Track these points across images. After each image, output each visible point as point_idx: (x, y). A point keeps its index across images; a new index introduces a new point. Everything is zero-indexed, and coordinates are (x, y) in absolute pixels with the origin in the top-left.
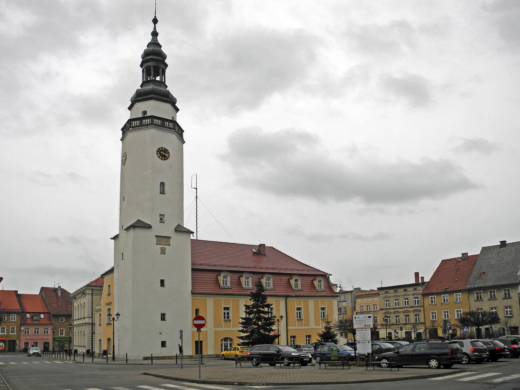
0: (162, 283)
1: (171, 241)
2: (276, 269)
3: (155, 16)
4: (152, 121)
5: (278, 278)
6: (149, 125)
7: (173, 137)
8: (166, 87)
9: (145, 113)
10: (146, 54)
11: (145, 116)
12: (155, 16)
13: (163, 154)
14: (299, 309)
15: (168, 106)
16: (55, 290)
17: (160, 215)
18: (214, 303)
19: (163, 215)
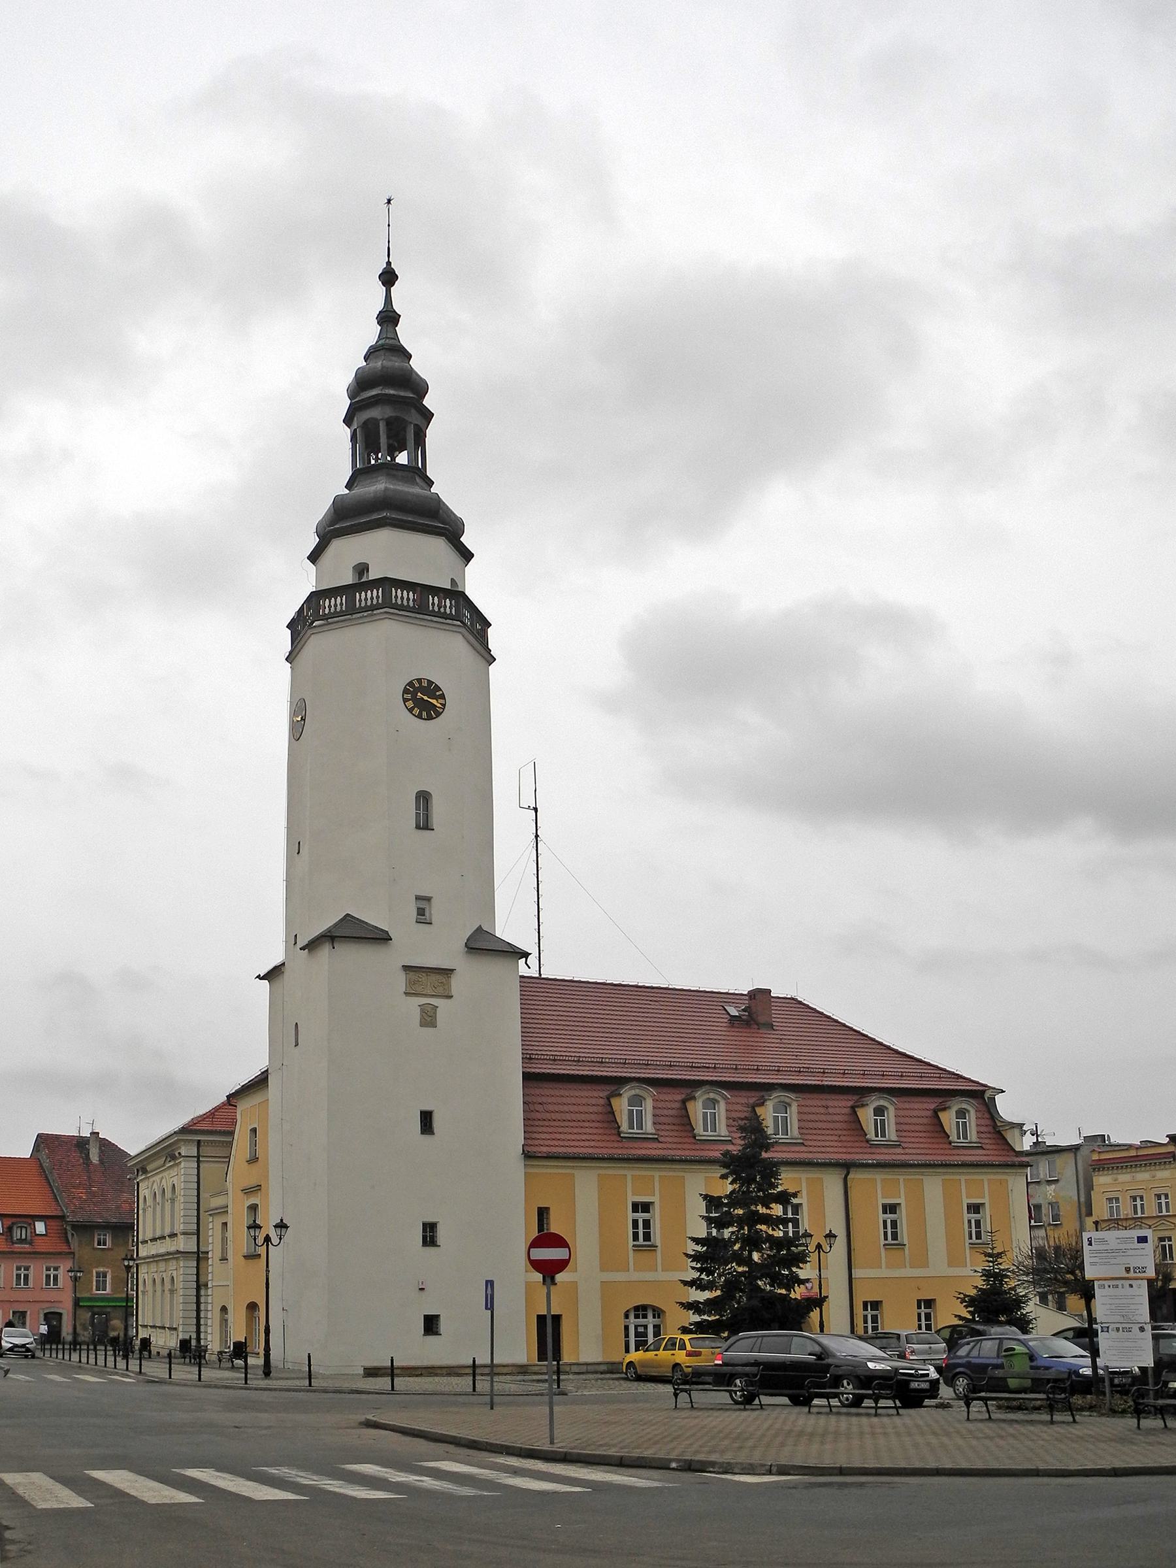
0: (427, 1121)
2: (809, 1071)
3: (389, 263)
8: (430, 483)
9: (362, 569)
10: (362, 384)
11: (362, 581)
12: (389, 263)
13: (424, 699)
15: (439, 545)
16: (81, 1144)
17: (418, 898)
19: (428, 899)
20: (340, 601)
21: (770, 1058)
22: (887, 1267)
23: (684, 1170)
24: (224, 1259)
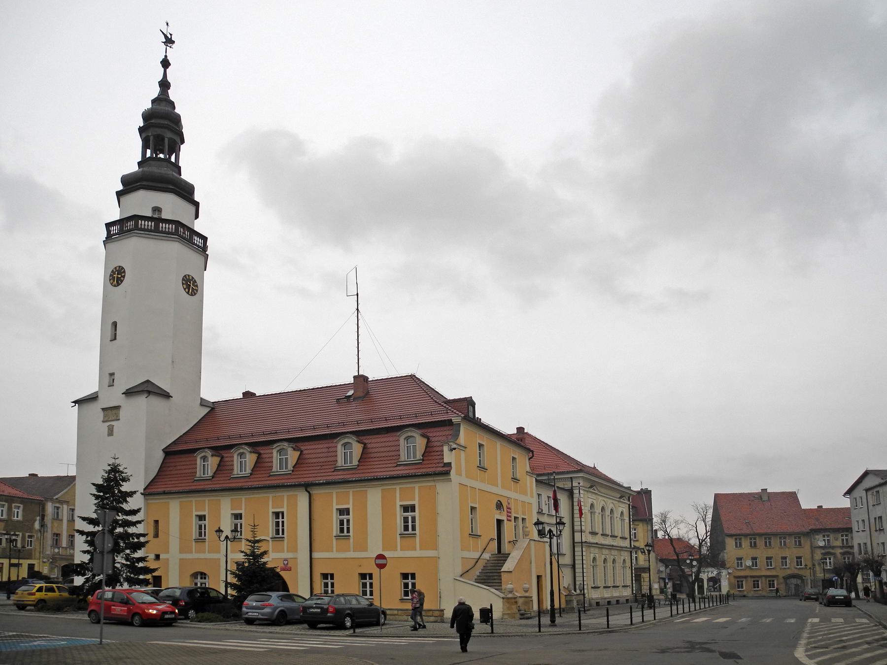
1: (122, 413)
3: (166, 56)
4: (157, 226)
5: (316, 545)
6: (172, 234)
7: (198, 258)
12: (166, 56)
14: (342, 512)
18: (181, 509)
20: (151, 224)
21: (389, 412)
22: (421, 549)
23: (365, 487)
24: (863, 521)
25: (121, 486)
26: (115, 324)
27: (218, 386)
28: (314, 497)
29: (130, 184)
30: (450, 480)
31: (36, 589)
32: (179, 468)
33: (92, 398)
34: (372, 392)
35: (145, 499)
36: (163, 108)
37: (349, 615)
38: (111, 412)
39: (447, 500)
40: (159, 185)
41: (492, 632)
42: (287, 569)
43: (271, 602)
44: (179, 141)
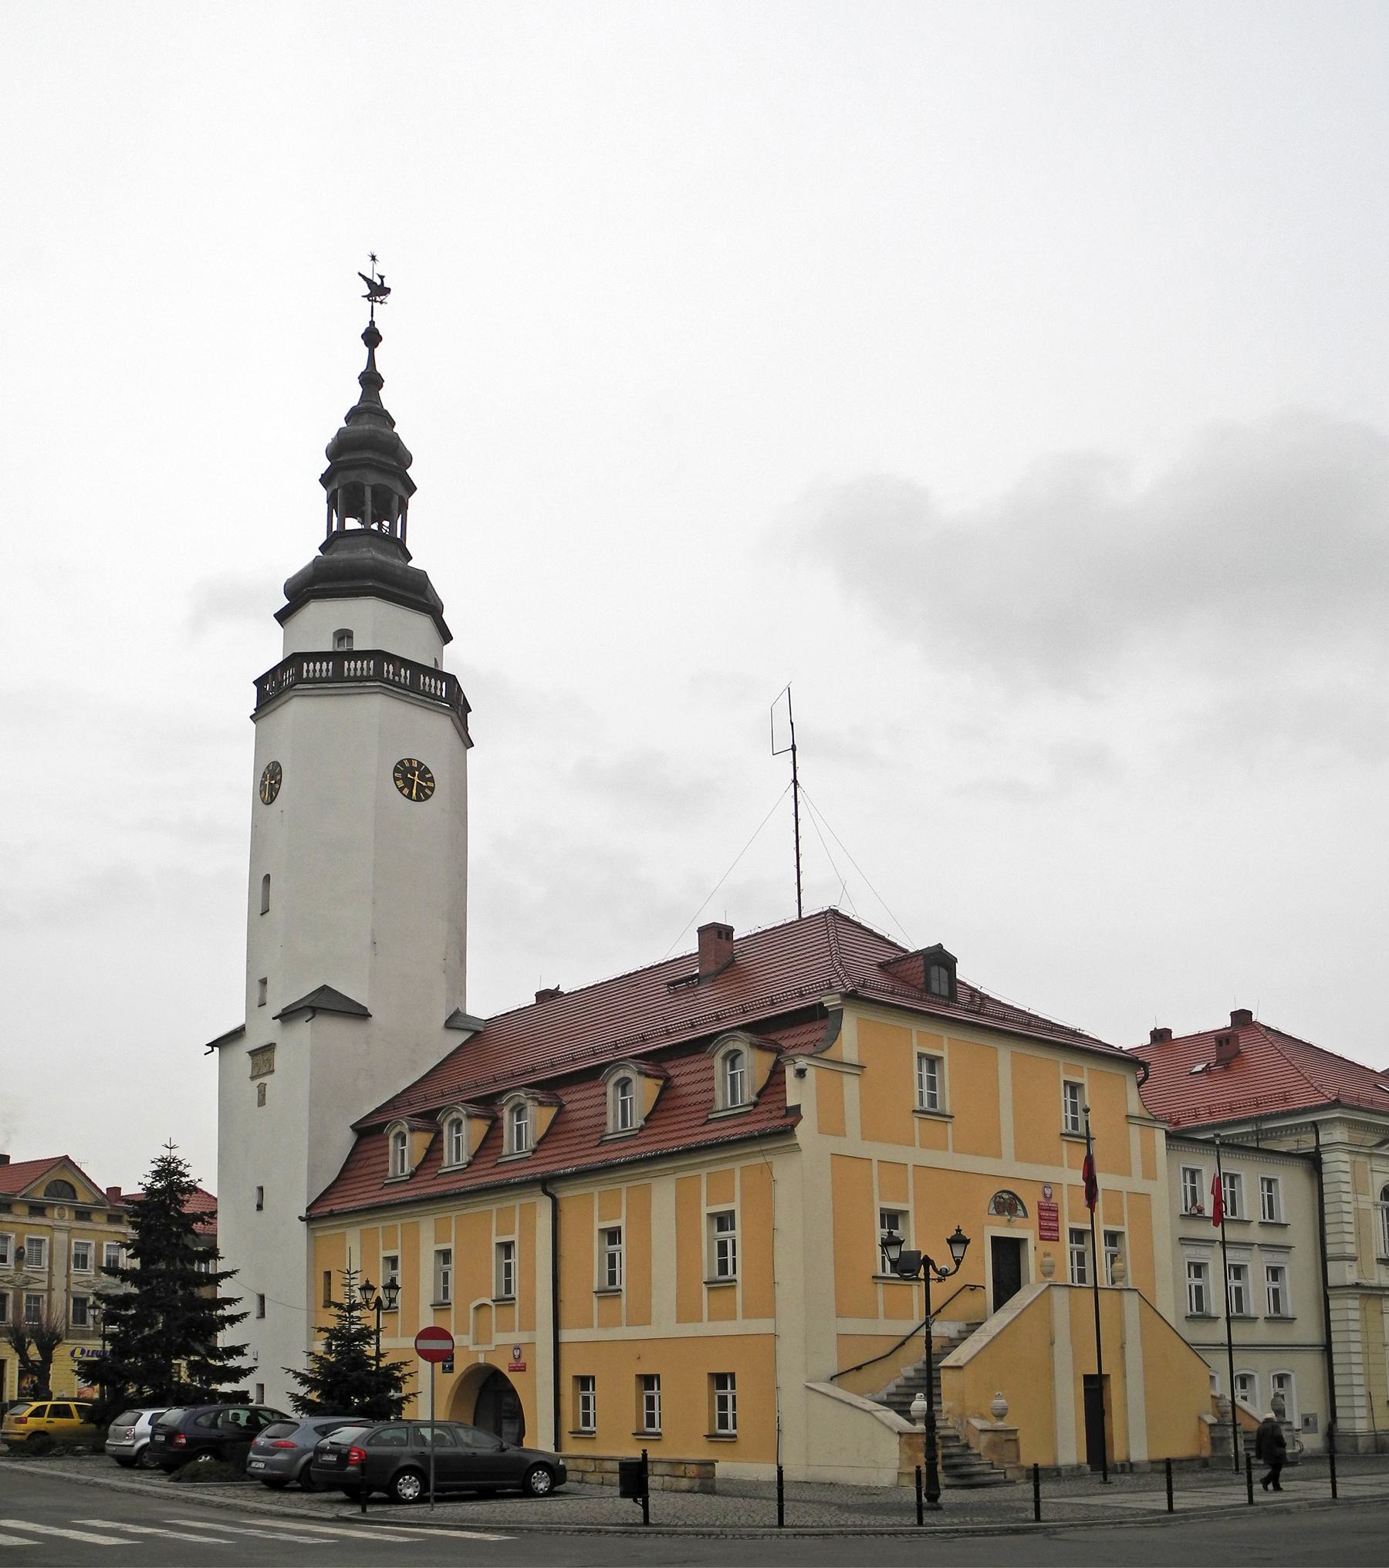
1: (279, 1058)
3: (372, 323)
4: (379, 669)
6: (368, 679)
7: (441, 725)
12: (372, 323)
13: (413, 780)
15: (424, 622)
20: (327, 668)
25: (181, 1203)
26: (267, 878)
27: (494, 990)
28: (564, 1206)
29: (303, 591)
30: (796, 1148)
31: (31, 1409)
32: (371, 1162)
33: (237, 1034)
34: (740, 959)
35: (311, 1231)
36: (366, 426)
37: (409, 1470)
38: (263, 1054)
39: (801, 1199)
40: (345, 585)
41: (646, 1522)
42: (519, 1368)
43: (293, 1439)
44: (400, 490)
